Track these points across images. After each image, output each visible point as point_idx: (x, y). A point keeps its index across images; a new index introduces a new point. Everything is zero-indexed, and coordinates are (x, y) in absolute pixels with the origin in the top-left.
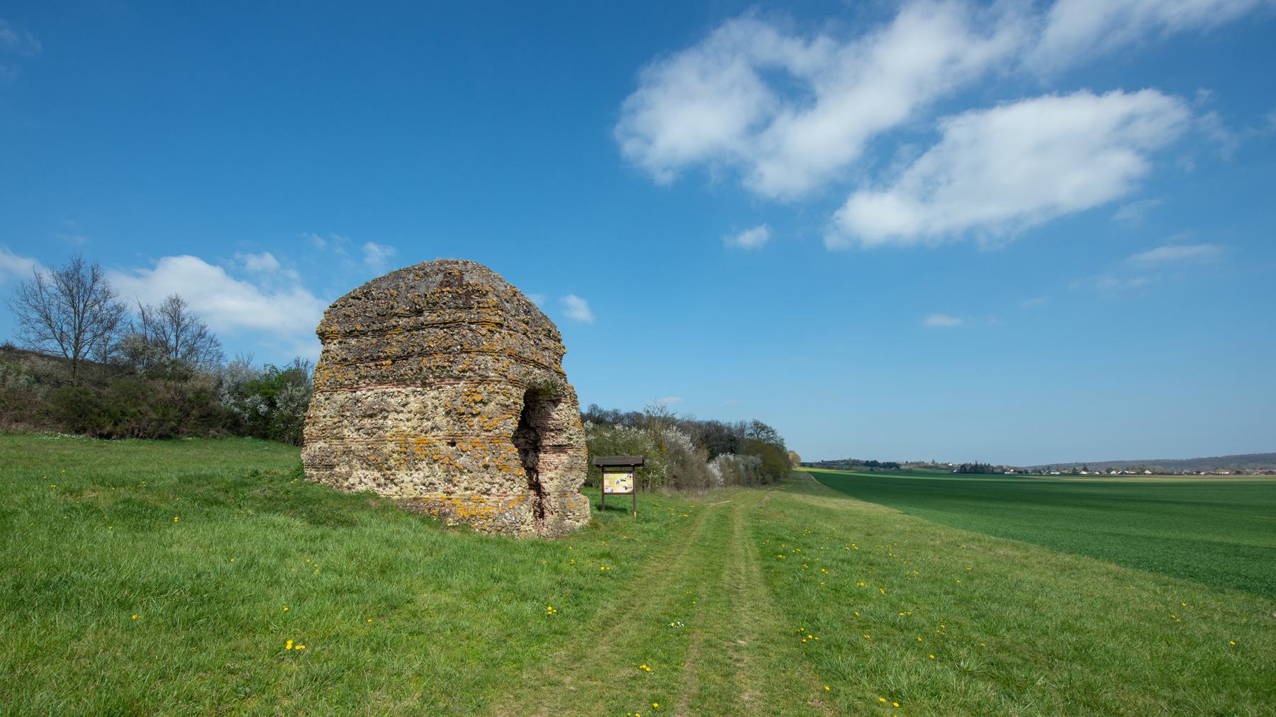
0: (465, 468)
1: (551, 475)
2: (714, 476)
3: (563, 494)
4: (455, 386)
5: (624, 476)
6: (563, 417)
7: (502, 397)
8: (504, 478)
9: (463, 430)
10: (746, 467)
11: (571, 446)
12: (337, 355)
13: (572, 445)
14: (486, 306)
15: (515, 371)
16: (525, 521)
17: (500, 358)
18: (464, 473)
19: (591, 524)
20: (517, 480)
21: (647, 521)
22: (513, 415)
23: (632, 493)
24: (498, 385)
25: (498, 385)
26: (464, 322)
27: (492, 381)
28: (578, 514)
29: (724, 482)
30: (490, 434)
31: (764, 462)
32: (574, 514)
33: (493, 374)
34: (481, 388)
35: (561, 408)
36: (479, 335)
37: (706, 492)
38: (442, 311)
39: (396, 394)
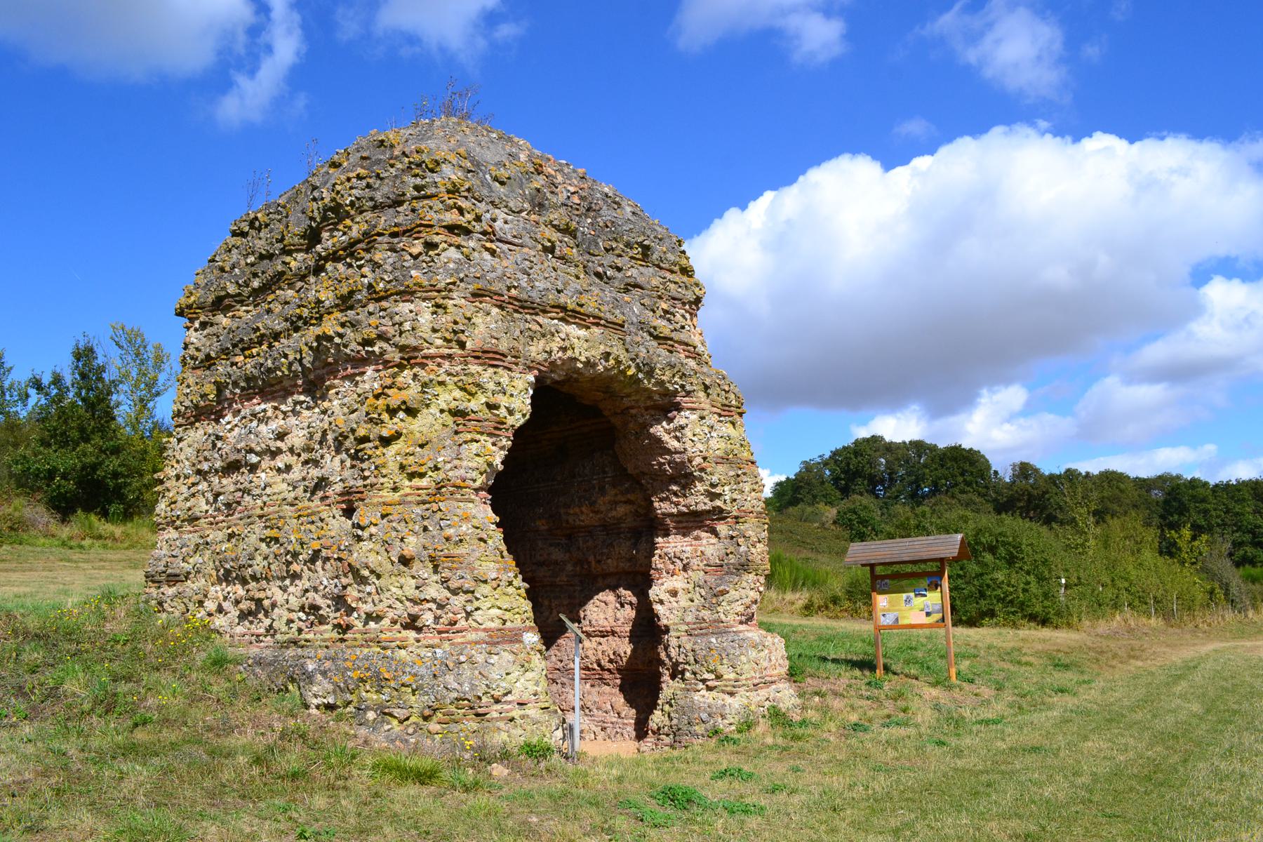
7: (458, 394)
9: (365, 478)
11: (719, 514)
28: (732, 676)
30: (424, 482)
35: (683, 422)
39: (270, 413)
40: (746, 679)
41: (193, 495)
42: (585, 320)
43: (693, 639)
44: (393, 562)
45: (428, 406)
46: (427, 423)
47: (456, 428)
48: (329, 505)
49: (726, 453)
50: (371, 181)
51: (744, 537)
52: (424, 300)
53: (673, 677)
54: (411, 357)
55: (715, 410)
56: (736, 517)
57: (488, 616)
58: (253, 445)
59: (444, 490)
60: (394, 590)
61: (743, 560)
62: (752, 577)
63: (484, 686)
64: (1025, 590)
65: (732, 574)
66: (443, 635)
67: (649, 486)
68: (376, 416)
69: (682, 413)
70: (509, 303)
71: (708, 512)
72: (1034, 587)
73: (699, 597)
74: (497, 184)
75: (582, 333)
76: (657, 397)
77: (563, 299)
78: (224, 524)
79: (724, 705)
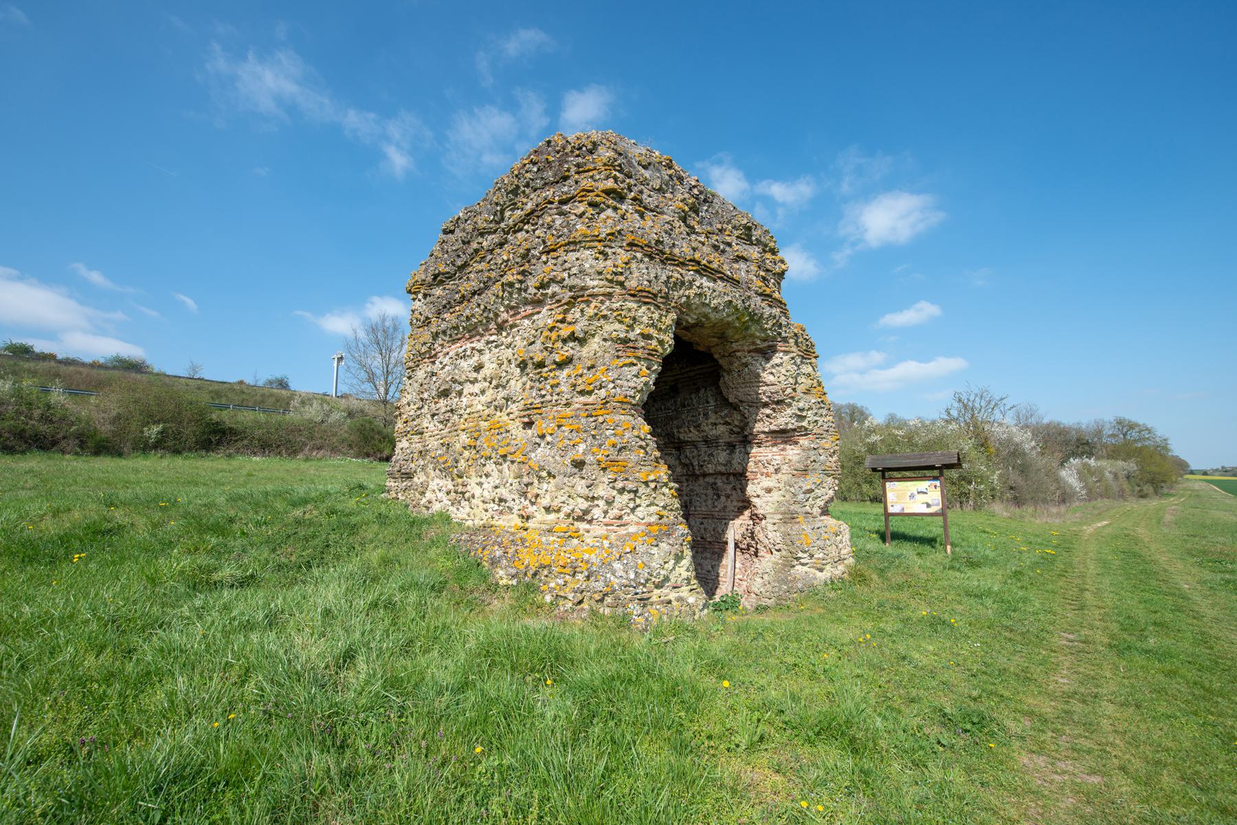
0: (542, 469)
1: (767, 483)
2: (1071, 487)
3: (790, 518)
4: (535, 317)
5: (923, 485)
6: (783, 378)
7: (617, 326)
8: (613, 488)
9: (544, 396)
10: (1116, 476)
13: (806, 429)
15: (642, 274)
17: (609, 251)
18: (543, 478)
19: (850, 574)
20: (642, 490)
21: (973, 565)
22: (639, 358)
23: (942, 514)
24: (608, 303)
25: (608, 303)
26: (552, 203)
27: (593, 296)
28: (821, 555)
29: (1087, 494)
30: (591, 399)
31: (1142, 470)
32: (812, 556)
33: (595, 283)
34: (575, 313)
37: (1063, 508)
41: (418, 416)
42: (712, 274)
47: (616, 354)
48: (513, 420)
55: (800, 353)
58: (457, 377)
63: (646, 574)
66: (609, 528)
67: (746, 411)
68: (551, 346)
69: (777, 355)
70: (657, 254)
71: (795, 430)
75: (711, 285)
77: (697, 256)
78: (439, 437)
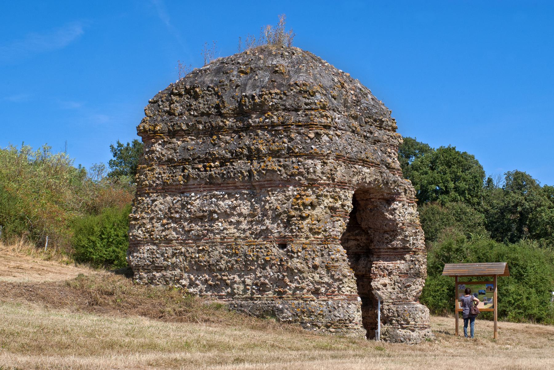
7: (331, 200)
12: (164, 155)
14: (314, 106)
16: (353, 320)
24: (327, 188)
34: (310, 192)
35: (395, 206)
36: (307, 138)
38: (270, 113)
40: (419, 325)
43: (396, 306)
44: (309, 268)
45: (320, 205)
46: (319, 211)
49: (411, 221)
50: (282, 96)
51: (418, 261)
52: (318, 159)
53: (384, 323)
54: (313, 184)
56: (414, 251)
57: (346, 290)
59: (329, 239)
60: (310, 278)
61: (417, 272)
62: (420, 280)
64: (528, 298)
65: (412, 277)
67: (372, 234)
72: (534, 297)
73: (398, 288)
74: (333, 99)
76: (385, 195)
79: (410, 335)
